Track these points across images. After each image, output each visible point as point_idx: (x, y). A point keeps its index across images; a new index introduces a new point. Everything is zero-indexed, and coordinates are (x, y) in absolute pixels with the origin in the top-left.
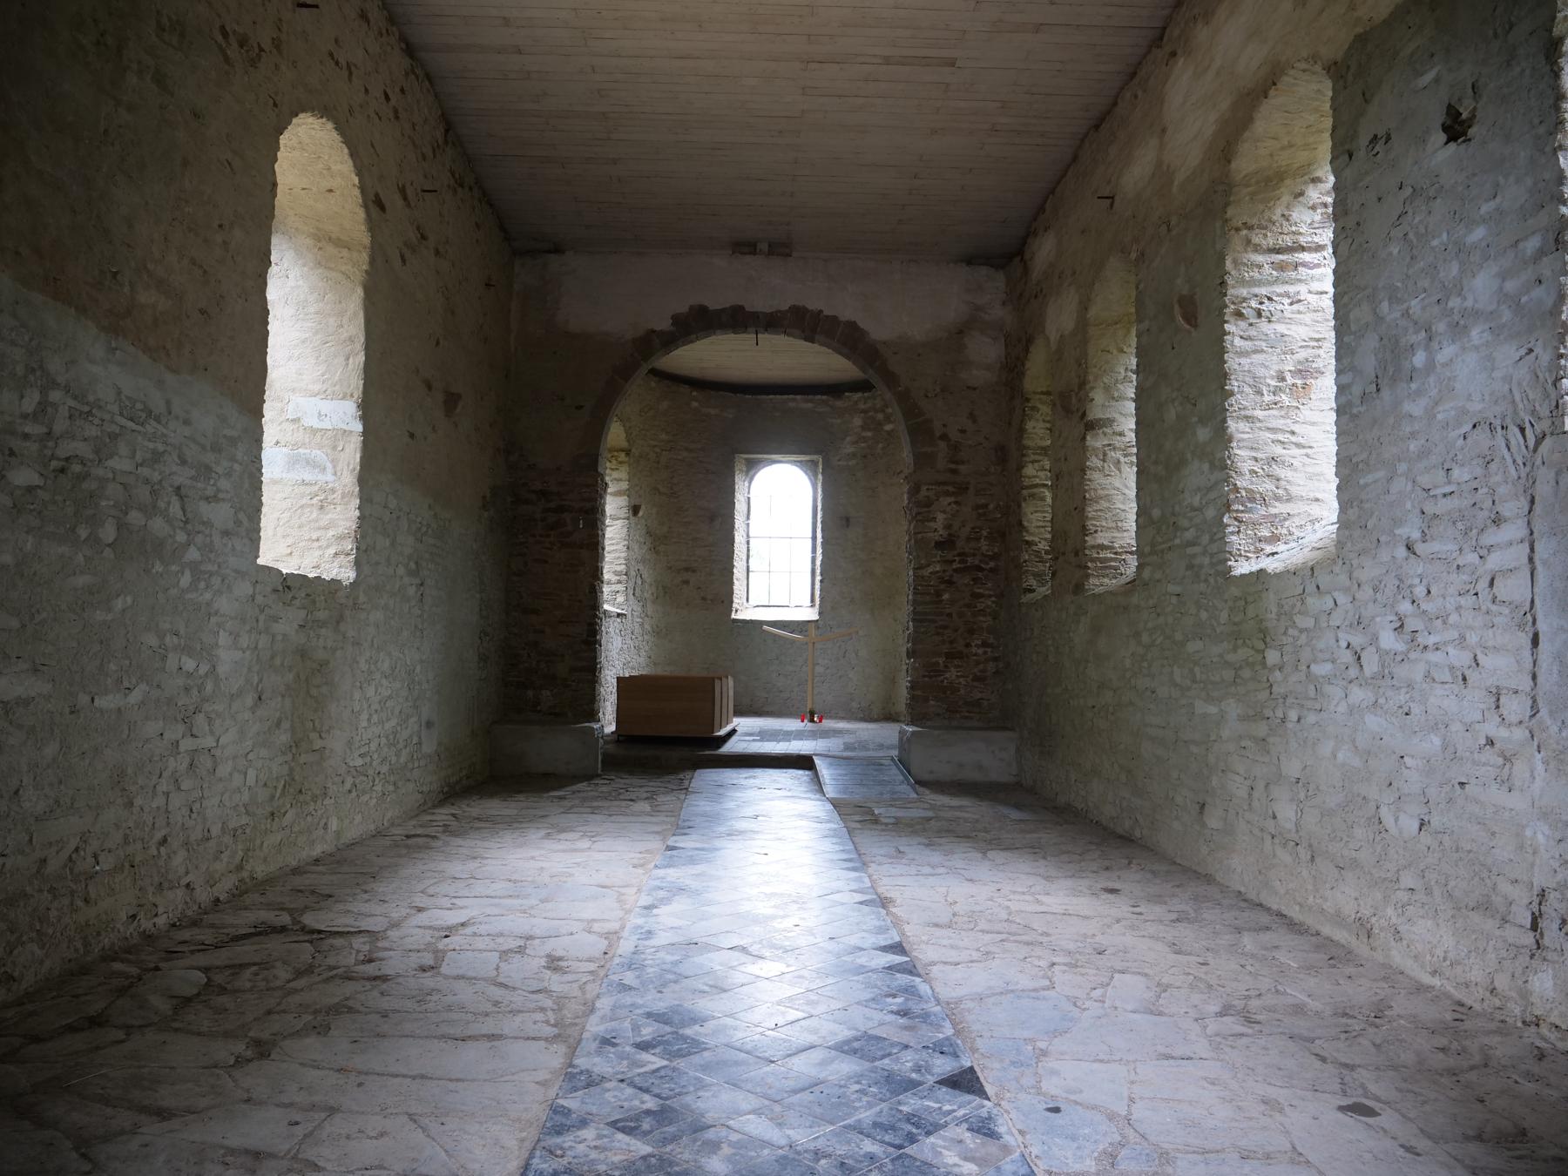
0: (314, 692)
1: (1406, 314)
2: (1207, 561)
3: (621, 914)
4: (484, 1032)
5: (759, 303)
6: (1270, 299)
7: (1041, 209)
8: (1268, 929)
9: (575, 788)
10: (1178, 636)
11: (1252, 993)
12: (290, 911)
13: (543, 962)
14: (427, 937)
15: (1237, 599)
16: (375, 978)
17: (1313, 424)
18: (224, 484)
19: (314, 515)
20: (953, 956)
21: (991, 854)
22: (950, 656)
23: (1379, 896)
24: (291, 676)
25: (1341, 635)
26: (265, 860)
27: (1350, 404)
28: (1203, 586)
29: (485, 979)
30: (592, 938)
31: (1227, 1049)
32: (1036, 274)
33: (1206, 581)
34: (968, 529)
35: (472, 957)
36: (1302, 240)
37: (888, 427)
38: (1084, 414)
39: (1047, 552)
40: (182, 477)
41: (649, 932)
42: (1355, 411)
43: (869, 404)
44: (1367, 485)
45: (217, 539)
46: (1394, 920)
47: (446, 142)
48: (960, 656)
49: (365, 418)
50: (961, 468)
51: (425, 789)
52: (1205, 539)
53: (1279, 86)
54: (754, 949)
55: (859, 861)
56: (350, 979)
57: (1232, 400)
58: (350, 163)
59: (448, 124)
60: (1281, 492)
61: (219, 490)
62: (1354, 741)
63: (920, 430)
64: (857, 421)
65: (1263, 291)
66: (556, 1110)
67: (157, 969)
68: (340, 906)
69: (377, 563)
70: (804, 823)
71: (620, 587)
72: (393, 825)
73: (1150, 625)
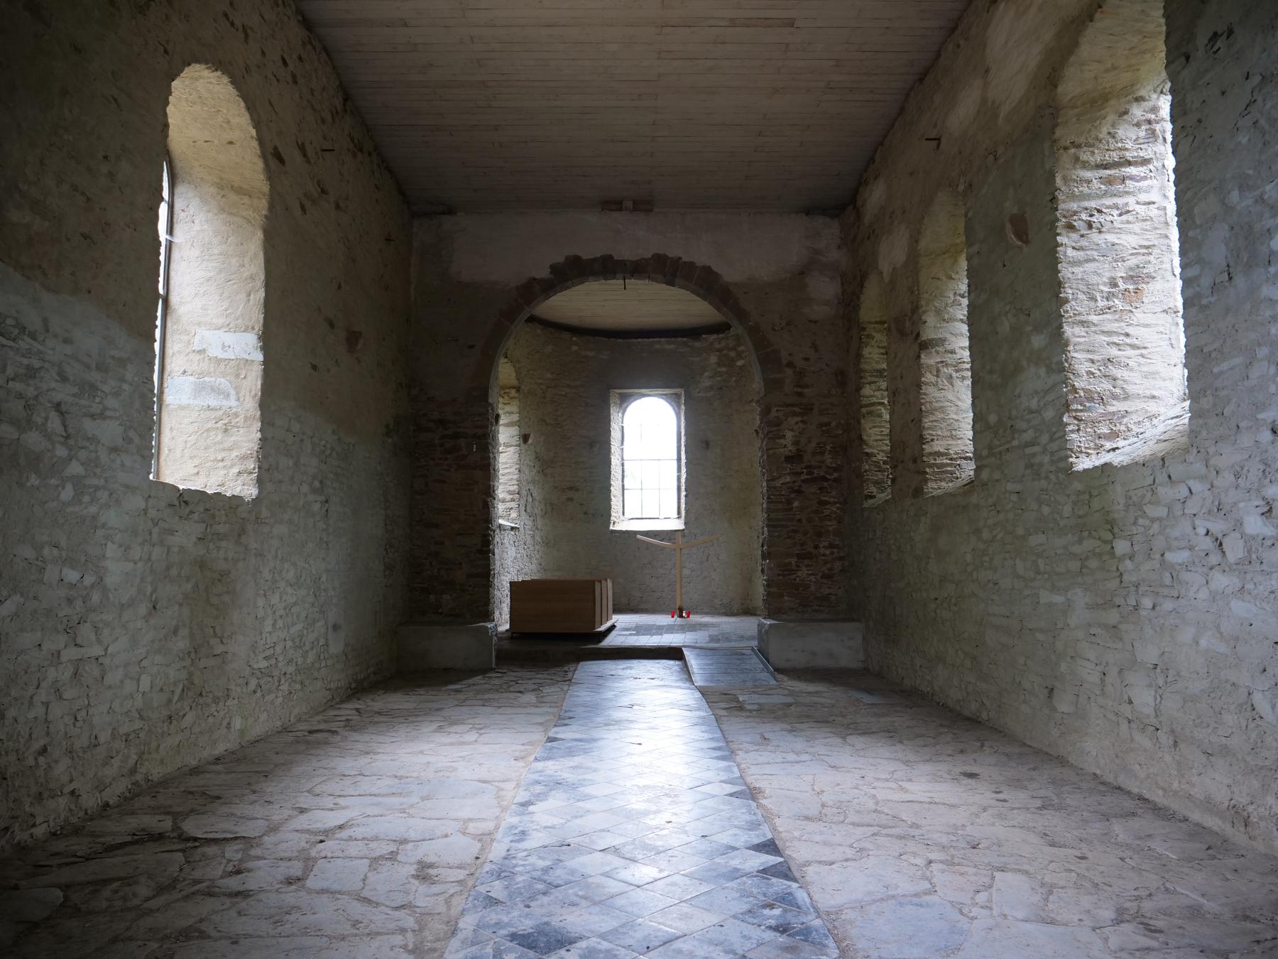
0: (215, 600)
1: (1261, 200)
2: (1047, 459)
5: (625, 252)
6: (1099, 211)
8: (1134, 814)
9: (470, 681)
11: (1144, 893)
12: (176, 816)
13: (412, 870)
14: (301, 841)
15: (1079, 493)
16: (238, 894)
17: (1147, 326)
18: (111, 402)
20: (826, 854)
21: (851, 739)
23: (1256, 784)
24: (189, 586)
25: (1197, 522)
26: (162, 761)
27: (1199, 296)
28: (1043, 483)
29: (349, 893)
30: (464, 840)
32: (868, 218)
33: (1047, 478)
34: (813, 444)
35: (340, 868)
36: (1128, 155)
37: (739, 363)
38: (918, 335)
39: (885, 463)
40: (63, 393)
41: (523, 833)
42: (1204, 302)
43: (723, 344)
44: (1221, 373)
45: (104, 457)
47: (345, 111)
51: (332, 686)
52: (1044, 439)
53: (1105, 8)
54: (626, 851)
55: (726, 750)
56: (211, 895)
57: (1067, 307)
58: (247, 115)
60: (1118, 390)
61: (106, 409)
62: (1218, 627)
63: (769, 359)
64: (713, 359)
67: (16, 887)
68: (225, 809)
69: (280, 482)
70: (676, 711)
71: (513, 505)
72: (299, 720)
73: (990, 522)
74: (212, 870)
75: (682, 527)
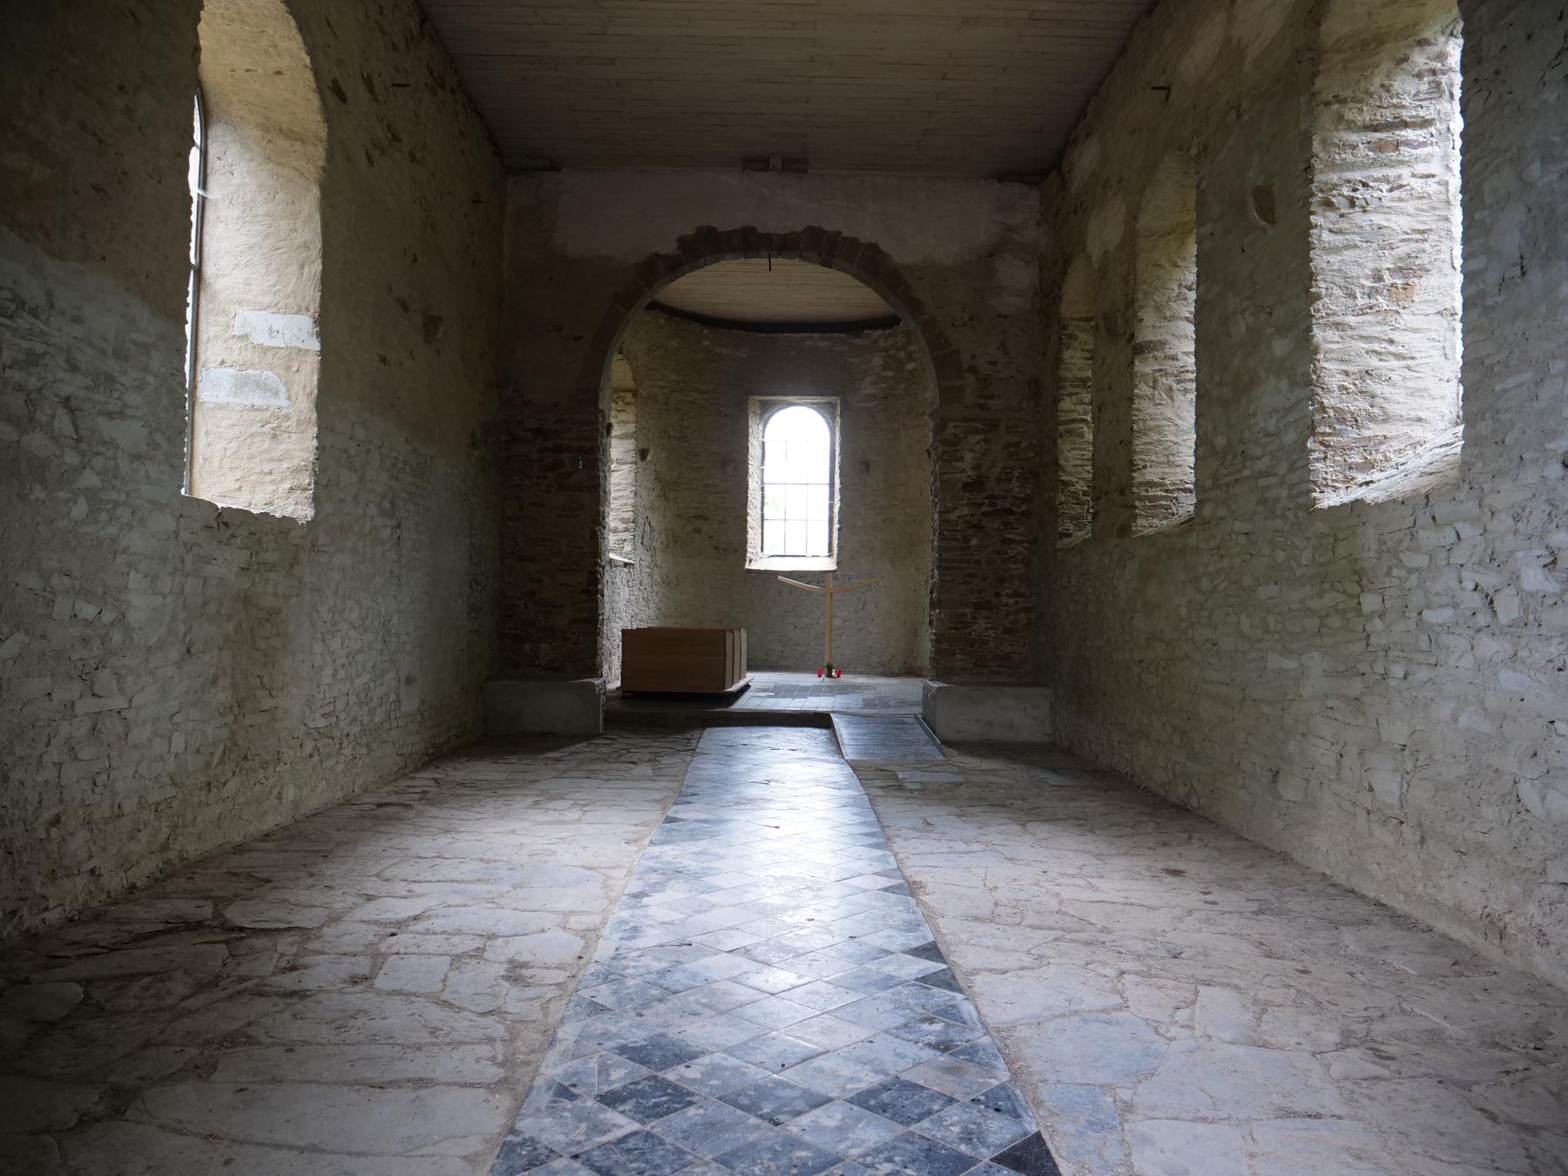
0: (262, 644)
2: (1284, 493)
3: (604, 903)
4: (410, 1075)
5: (771, 224)
6: (1365, 185)
7: (1083, 114)
8: (1368, 922)
9: (573, 748)
11: (1374, 1014)
12: (217, 902)
14: (369, 934)
15: (1322, 536)
16: (293, 994)
17: (1416, 331)
18: (133, 398)
19: (266, 445)
20: (998, 960)
21: (1032, 827)
22: (978, 607)
23: (1516, 889)
24: (230, 627)
25: (1465, 574)
26: (199, 837)
27: (1483, 294)
28: (1278, 523)
29: (425, 996)
31: (1365, 1101)
33: (1283, 516)
34: (998, 469)
36: (1405, 114)
37: (910, 366)
38: (1132, 336)
40: (73, 386)
41: (635, 929)
42: (1489, 302)
44: (1506, 391)
45: (124, 465)
46: (1538, 919)
50: (990, 402)
52: (1283, 468)
54: (759, 952)
55: (881, 836)
56: (260, 994)
57: (1319, 305)
58: (299, 38)
60: (1376, 410)
61: (125, 406)
62: (1482, 702)
63: (946, 361)
64: (878, 361)
65: (1357, 176)
67: (27, 981)
68: (276, 895)
69: (342, 501)
71: (628, 535)
72: (365, 791)
73: (1211, 569)
75: (833, 567)
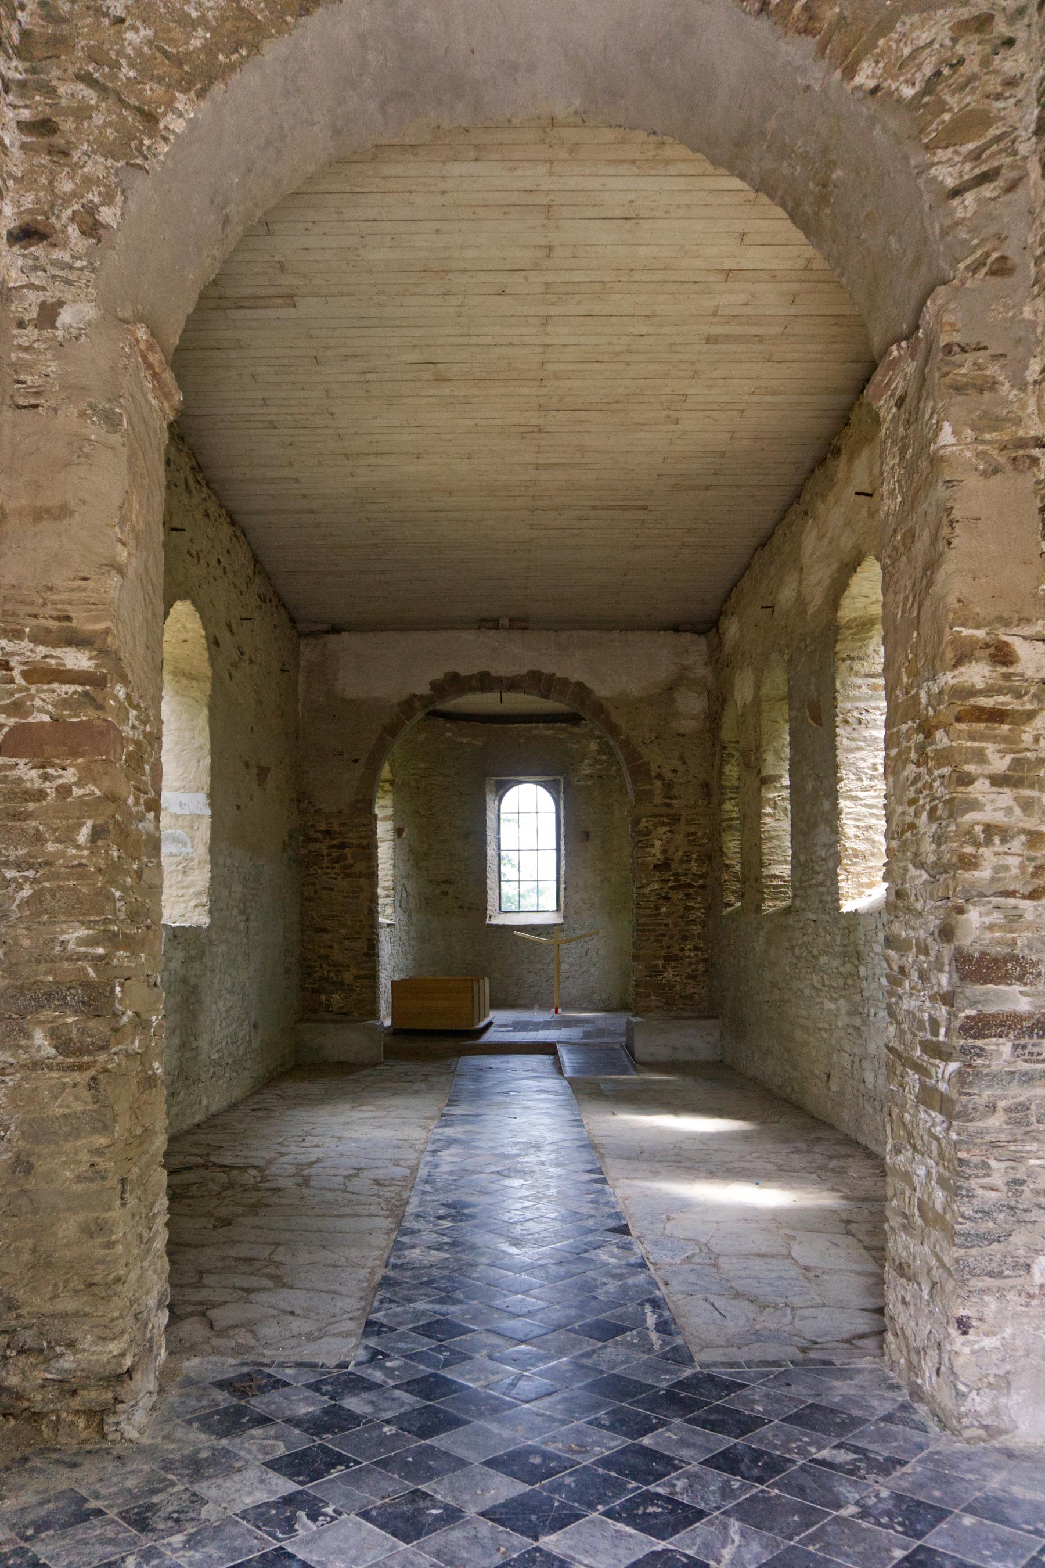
5: (501, 669)
10: (815, 952)
22: (667, 959)
32: (727, 647)
38: (759, 772)
48: (676, 958)
49: (212, 805)
57: (842, 784)
59: (256, 560)
64: (593, 746)
66: (396, 1242)
74: (249, 1177)
75: (560, 921)
